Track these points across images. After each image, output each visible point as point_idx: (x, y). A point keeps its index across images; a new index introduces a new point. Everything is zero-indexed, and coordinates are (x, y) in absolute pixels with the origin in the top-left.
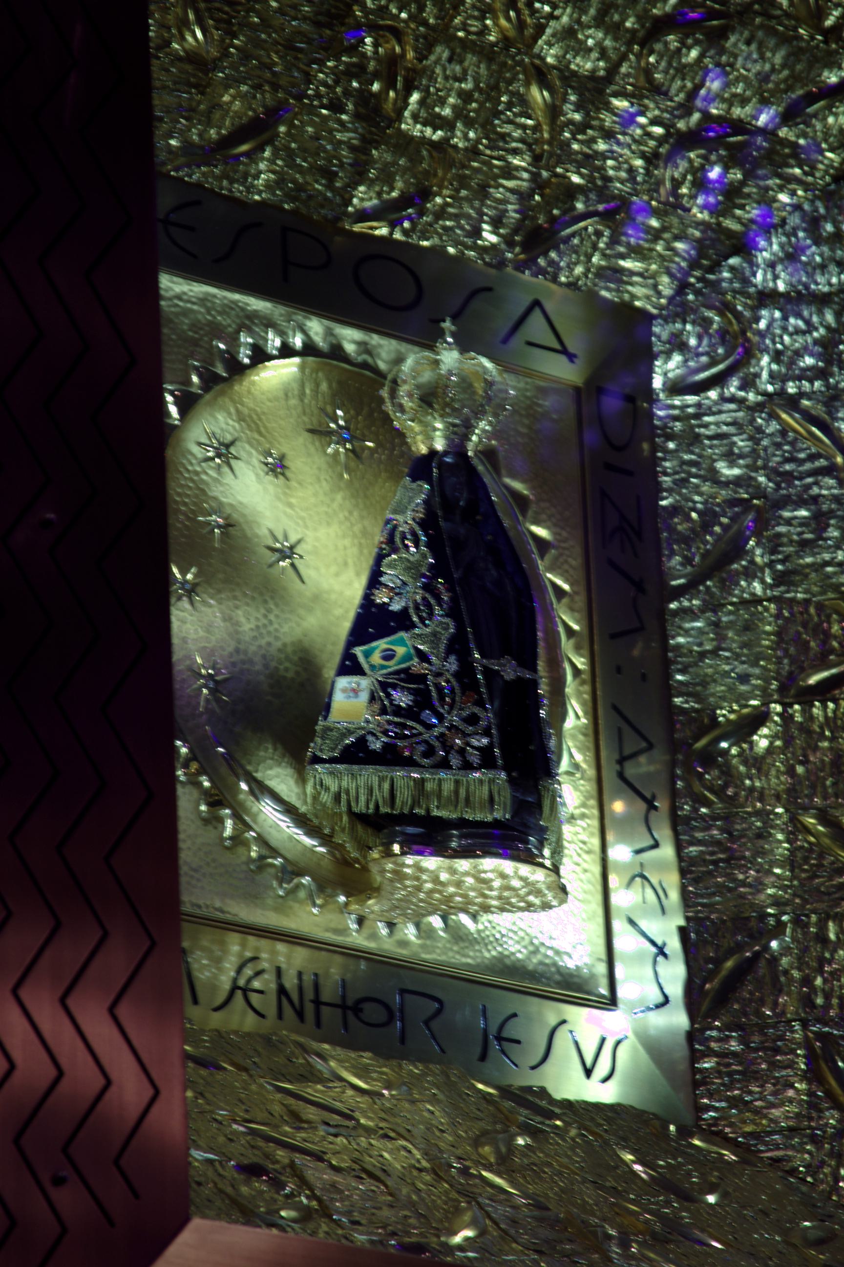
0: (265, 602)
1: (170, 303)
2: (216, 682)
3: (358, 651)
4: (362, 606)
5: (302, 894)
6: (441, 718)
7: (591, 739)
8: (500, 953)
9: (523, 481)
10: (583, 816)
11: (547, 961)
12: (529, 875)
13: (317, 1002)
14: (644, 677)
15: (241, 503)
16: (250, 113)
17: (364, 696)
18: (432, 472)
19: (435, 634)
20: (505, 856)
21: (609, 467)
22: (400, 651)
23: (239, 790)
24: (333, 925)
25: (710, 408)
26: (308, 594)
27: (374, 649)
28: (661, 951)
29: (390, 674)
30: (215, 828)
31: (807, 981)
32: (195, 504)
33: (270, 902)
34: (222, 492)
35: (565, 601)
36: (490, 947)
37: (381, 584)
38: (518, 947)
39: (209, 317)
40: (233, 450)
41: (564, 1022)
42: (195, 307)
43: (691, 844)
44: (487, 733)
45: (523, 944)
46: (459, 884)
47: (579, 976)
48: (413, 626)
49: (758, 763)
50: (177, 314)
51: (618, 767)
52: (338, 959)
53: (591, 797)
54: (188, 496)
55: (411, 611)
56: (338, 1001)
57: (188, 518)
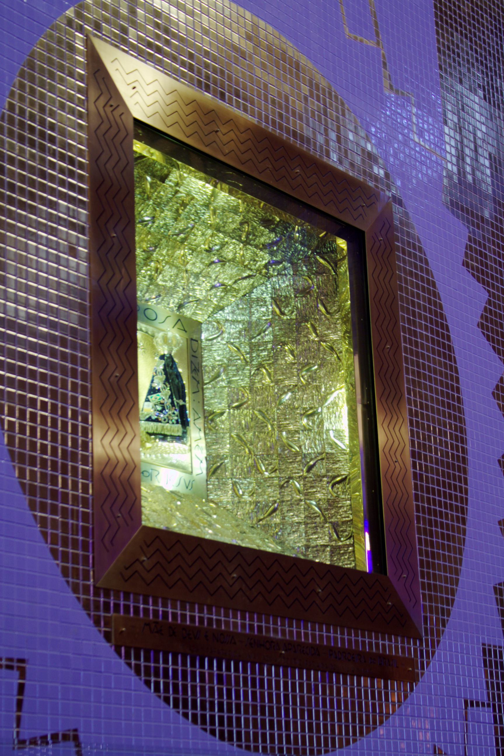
3: (149, 397)
17: (151, 407)
21: (193, 356)
22: (158, 397)
31: (232, 470)
49: (222, 422)
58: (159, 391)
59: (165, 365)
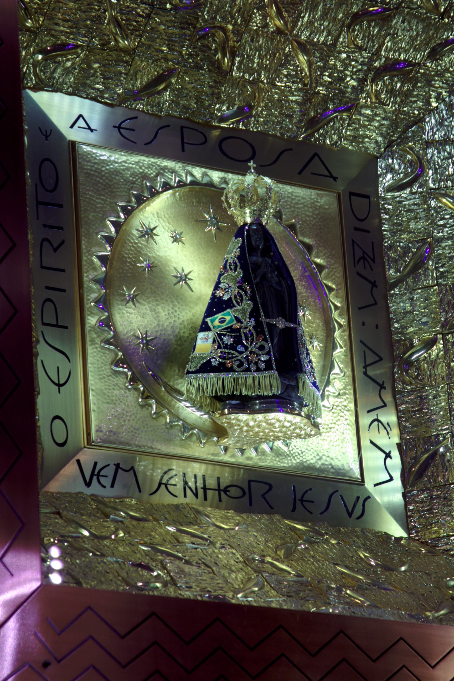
0: (173, 301)
1: (120, 165)
2: (147, 341)
3: (208, 320)
4: (211, 299)
5: (194, 438)
6: (246, 348)
7: (349, 357)
8: (302, 460)
9: (310, 238)
10: (345, 394)
11: (327, 463)
12: (292, 420)
13: (205, 489)
14: (377, 326)
15: (159, 256)
16: (156, 73)
17: (211, 341)
18: (244, 233)
19: (244, 309)
20: (281, 411)
22: (228, 318)
23: (161, 391)
24: (212, 452)
25: (406, 198)
26: (195, 296)
27: (216, 318)
28: (388, 455)
29: (223, 329)
30: (147, 409)
32: (135, 258)
33: (177, 442)
34: (149, 251)
35: (333, 293)
36: (296, 458)
37: (219, 288)
38: (311, 457)
39: (141, 171)
40: (155, 232)
41: (337, 491)
42: (134, 166)
43: (402, 404)
44: (268, 353)
45: (313, 455)
46: (259, 426)
47: (344, 469)
48: (234, 306)
50: (124, 170)
51: (364, 370)
52: (227, 469)
53: (350, 385)
54: (131, 254)
55: (233, 298)
56: (217, 488)
57: (131, 264)
58: (229, 304)
59: (242, 248)
